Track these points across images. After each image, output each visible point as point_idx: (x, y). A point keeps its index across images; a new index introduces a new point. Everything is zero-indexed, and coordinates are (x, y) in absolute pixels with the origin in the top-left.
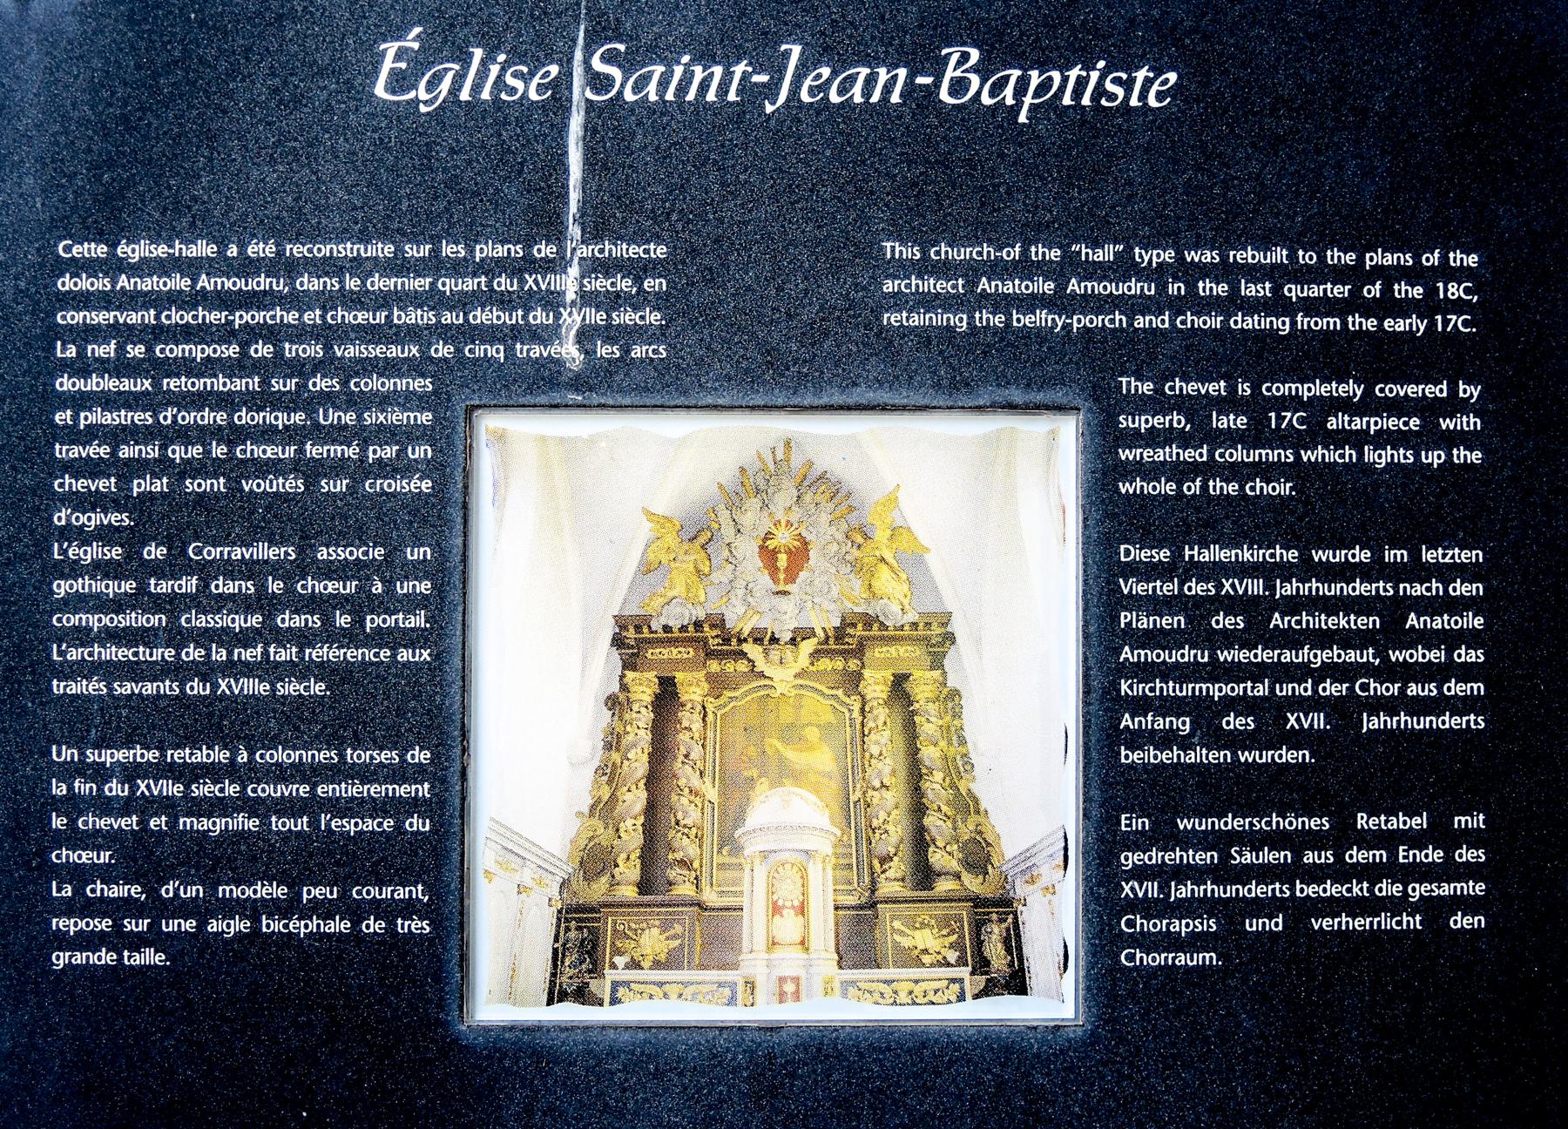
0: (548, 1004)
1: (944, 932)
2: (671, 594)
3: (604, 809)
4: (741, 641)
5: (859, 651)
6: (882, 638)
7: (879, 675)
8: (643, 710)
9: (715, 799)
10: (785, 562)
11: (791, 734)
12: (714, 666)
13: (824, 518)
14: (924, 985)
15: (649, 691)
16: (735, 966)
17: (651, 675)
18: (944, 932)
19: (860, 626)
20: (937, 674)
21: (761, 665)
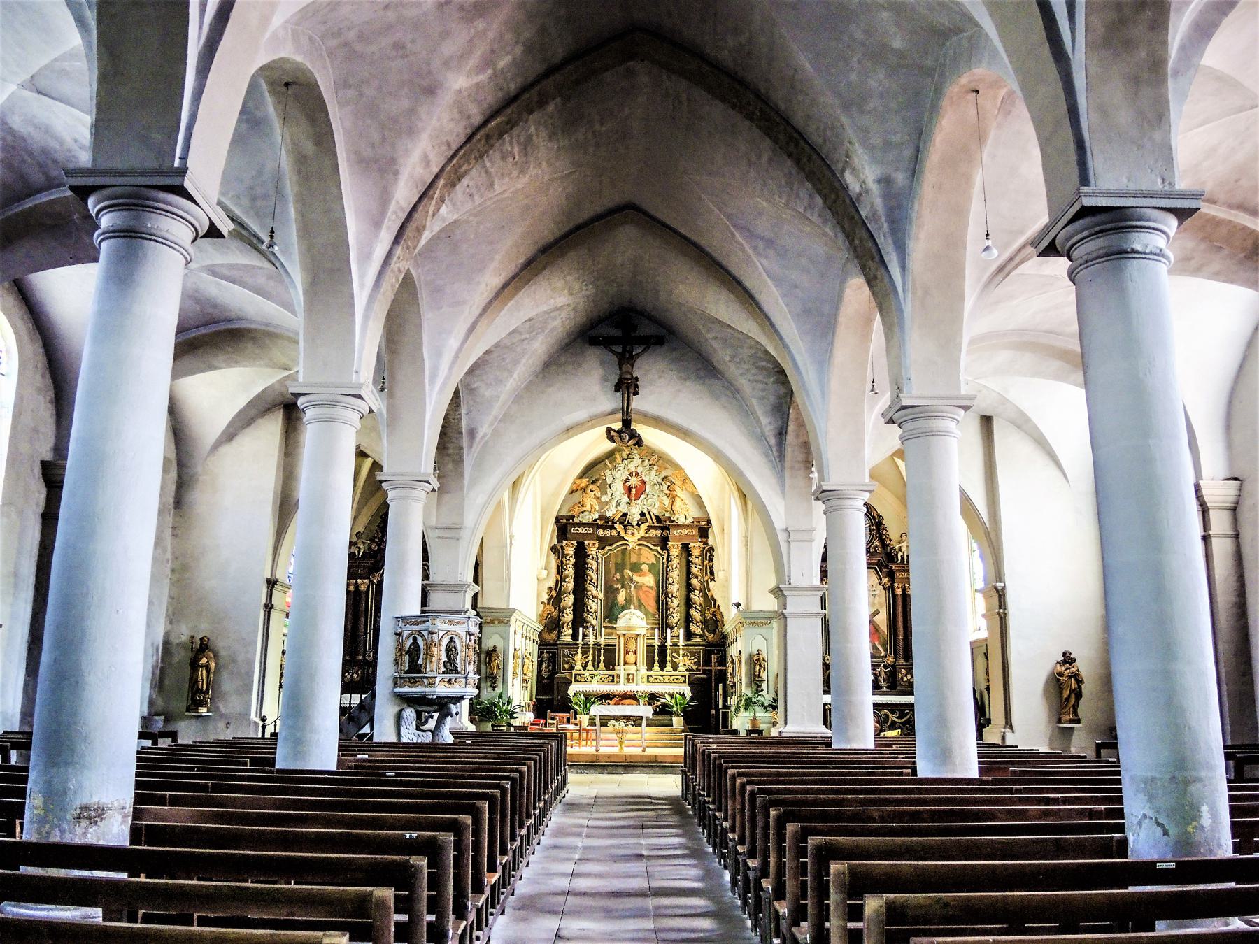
0: (358, 447)
10: (634, 492)
11: (636, 568)
13: (653, 472)
21: (622, 534)
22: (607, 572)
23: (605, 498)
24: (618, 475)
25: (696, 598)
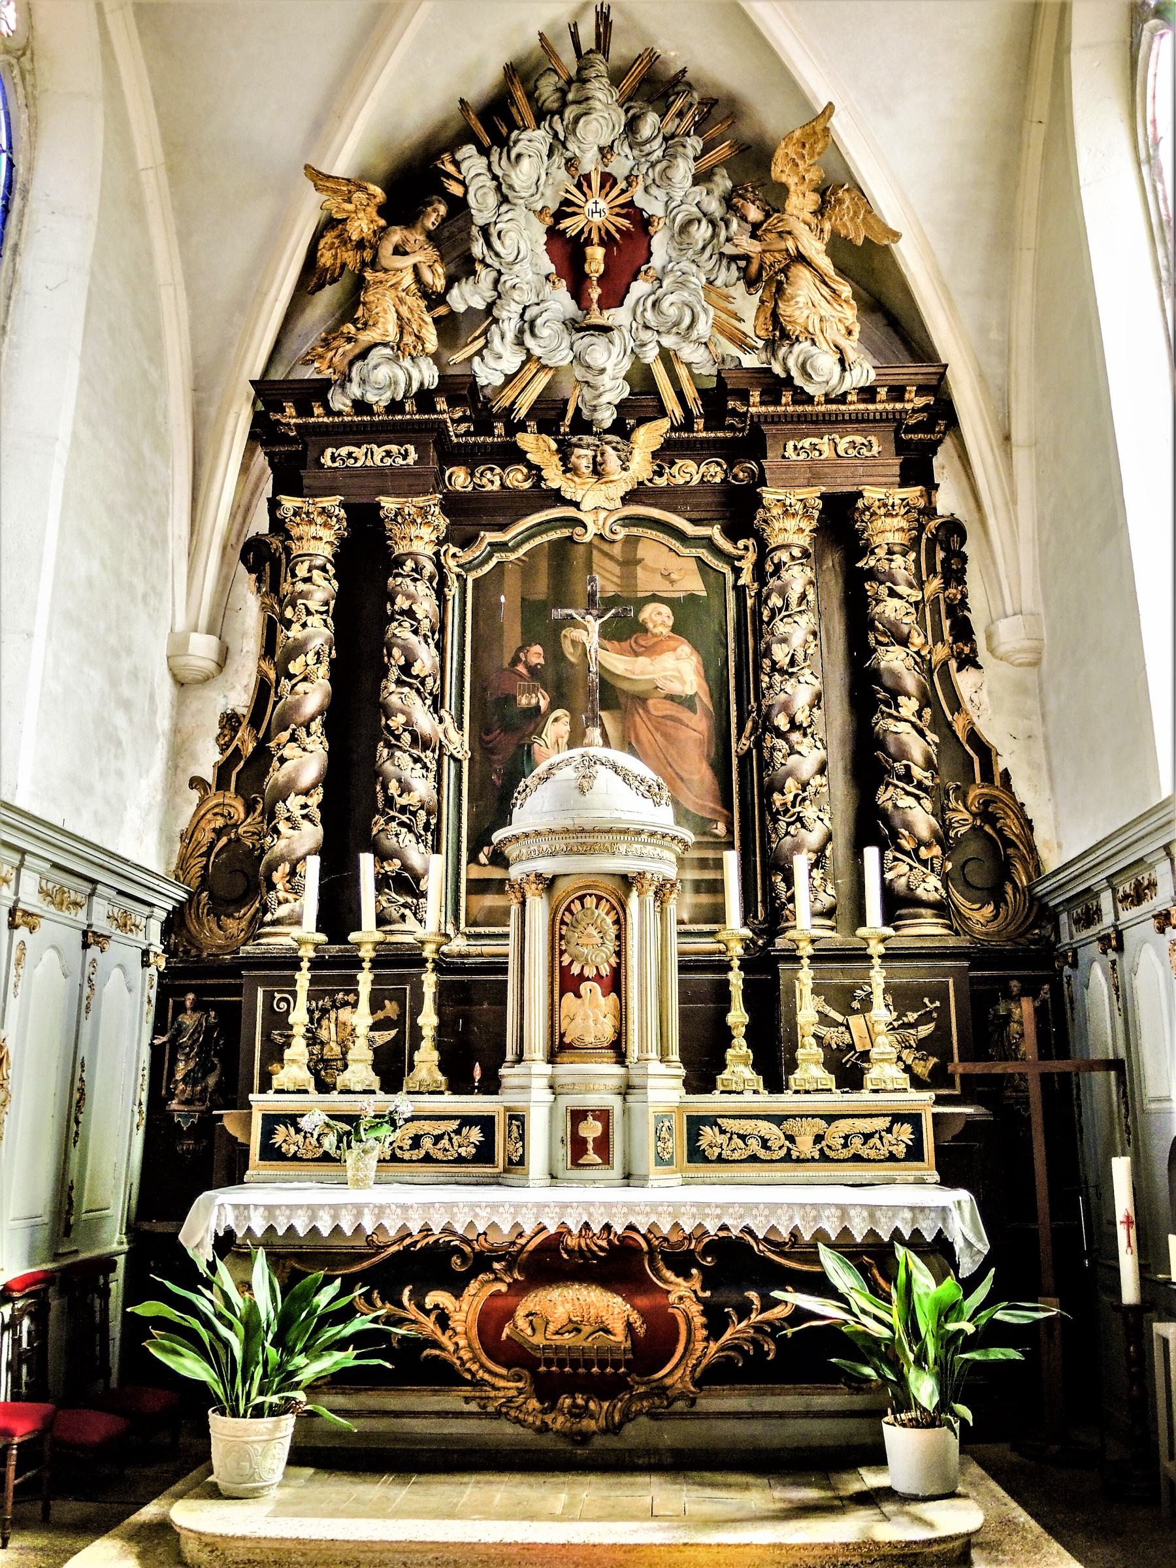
1: (912, 1017)
2: (366, 337)
3: (247, 770)
4: (515, 427)
5: (751, 445)
6: (802, 419)
7: (793, 497)
8: (317, 575)
9: (464, 754)
10: (599, 263)
12: (460, 479)
13: (683, 170)
14: (844, 1126)
15: (328, 535)
16: (491, 1085)
17: (331, 502)
18: (912, 1017)
19: (755, 397)
20: (913, 493)
21: (554, 478)
22: (485, 640)
23: (466, 297)
24: (523, 176)
25: (907, 735)
